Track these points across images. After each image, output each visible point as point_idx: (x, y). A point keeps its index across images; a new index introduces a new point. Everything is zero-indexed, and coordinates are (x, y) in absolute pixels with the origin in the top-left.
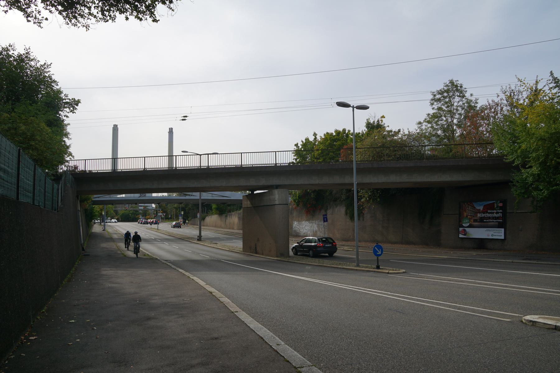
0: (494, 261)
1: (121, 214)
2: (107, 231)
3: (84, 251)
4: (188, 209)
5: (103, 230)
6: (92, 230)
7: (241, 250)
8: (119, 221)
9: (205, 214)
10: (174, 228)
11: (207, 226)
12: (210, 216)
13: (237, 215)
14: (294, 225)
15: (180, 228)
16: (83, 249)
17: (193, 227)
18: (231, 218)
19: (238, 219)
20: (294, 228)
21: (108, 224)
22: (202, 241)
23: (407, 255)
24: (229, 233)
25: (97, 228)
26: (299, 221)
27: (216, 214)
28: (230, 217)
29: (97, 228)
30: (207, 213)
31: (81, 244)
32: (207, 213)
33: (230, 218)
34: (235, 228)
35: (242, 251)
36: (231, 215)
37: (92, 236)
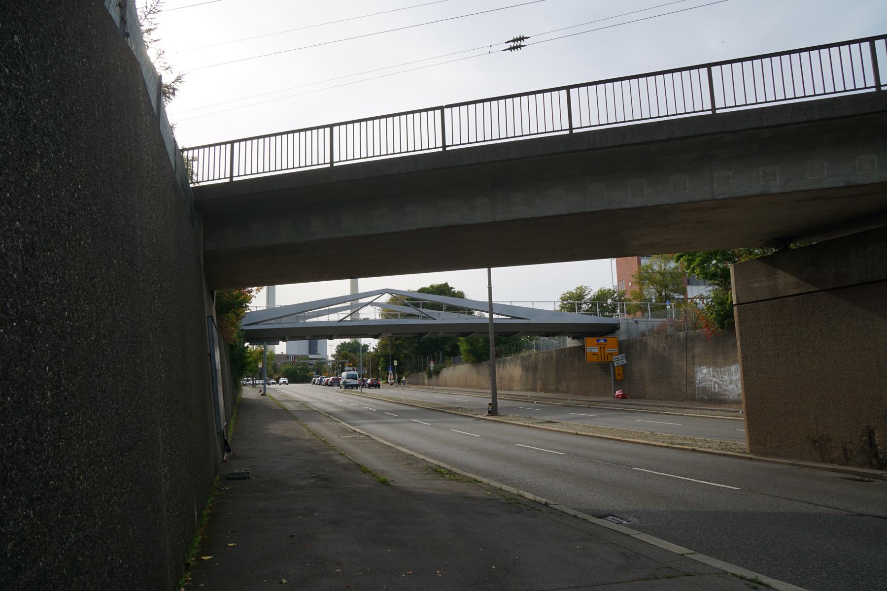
0: (712, 418)
1: (284, 370)
2: (270, 396)
3: (229, 451)
4: (403, 357)
5: (262, 395)
6: (241, 395)
7: (744, 444)
8: (290, 382)
9: (441, 365)
10: (369, 388)
11: (445, 386)
12: (452, 368)
13: (519, 362)
14: (699, 376)
15: (379, 388)
16: (226, 448)
17: (419, 388)
18: (503, 368)
19: (523, 370)
20: (700, 382)
21: (272, 386)
22: (500, 416)
23: (689, 414)
24: (517, 397)
25: (249, 392)
26: (715, 364)
27: (467, 361)
28: (501, 366)
29: (249, 392)
30: (443, 362)
31: (221, 434)
32: (443, 362)
33: (501, 369)
34: (515, 388)
35: (748, 451)
36: (504, 362)
37: (240, 407)
